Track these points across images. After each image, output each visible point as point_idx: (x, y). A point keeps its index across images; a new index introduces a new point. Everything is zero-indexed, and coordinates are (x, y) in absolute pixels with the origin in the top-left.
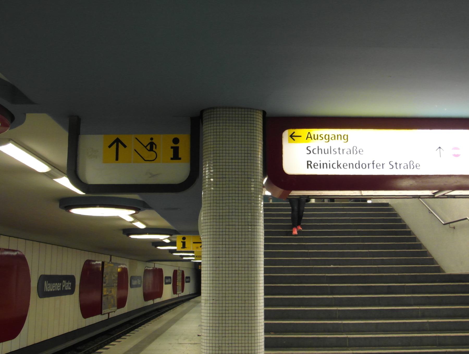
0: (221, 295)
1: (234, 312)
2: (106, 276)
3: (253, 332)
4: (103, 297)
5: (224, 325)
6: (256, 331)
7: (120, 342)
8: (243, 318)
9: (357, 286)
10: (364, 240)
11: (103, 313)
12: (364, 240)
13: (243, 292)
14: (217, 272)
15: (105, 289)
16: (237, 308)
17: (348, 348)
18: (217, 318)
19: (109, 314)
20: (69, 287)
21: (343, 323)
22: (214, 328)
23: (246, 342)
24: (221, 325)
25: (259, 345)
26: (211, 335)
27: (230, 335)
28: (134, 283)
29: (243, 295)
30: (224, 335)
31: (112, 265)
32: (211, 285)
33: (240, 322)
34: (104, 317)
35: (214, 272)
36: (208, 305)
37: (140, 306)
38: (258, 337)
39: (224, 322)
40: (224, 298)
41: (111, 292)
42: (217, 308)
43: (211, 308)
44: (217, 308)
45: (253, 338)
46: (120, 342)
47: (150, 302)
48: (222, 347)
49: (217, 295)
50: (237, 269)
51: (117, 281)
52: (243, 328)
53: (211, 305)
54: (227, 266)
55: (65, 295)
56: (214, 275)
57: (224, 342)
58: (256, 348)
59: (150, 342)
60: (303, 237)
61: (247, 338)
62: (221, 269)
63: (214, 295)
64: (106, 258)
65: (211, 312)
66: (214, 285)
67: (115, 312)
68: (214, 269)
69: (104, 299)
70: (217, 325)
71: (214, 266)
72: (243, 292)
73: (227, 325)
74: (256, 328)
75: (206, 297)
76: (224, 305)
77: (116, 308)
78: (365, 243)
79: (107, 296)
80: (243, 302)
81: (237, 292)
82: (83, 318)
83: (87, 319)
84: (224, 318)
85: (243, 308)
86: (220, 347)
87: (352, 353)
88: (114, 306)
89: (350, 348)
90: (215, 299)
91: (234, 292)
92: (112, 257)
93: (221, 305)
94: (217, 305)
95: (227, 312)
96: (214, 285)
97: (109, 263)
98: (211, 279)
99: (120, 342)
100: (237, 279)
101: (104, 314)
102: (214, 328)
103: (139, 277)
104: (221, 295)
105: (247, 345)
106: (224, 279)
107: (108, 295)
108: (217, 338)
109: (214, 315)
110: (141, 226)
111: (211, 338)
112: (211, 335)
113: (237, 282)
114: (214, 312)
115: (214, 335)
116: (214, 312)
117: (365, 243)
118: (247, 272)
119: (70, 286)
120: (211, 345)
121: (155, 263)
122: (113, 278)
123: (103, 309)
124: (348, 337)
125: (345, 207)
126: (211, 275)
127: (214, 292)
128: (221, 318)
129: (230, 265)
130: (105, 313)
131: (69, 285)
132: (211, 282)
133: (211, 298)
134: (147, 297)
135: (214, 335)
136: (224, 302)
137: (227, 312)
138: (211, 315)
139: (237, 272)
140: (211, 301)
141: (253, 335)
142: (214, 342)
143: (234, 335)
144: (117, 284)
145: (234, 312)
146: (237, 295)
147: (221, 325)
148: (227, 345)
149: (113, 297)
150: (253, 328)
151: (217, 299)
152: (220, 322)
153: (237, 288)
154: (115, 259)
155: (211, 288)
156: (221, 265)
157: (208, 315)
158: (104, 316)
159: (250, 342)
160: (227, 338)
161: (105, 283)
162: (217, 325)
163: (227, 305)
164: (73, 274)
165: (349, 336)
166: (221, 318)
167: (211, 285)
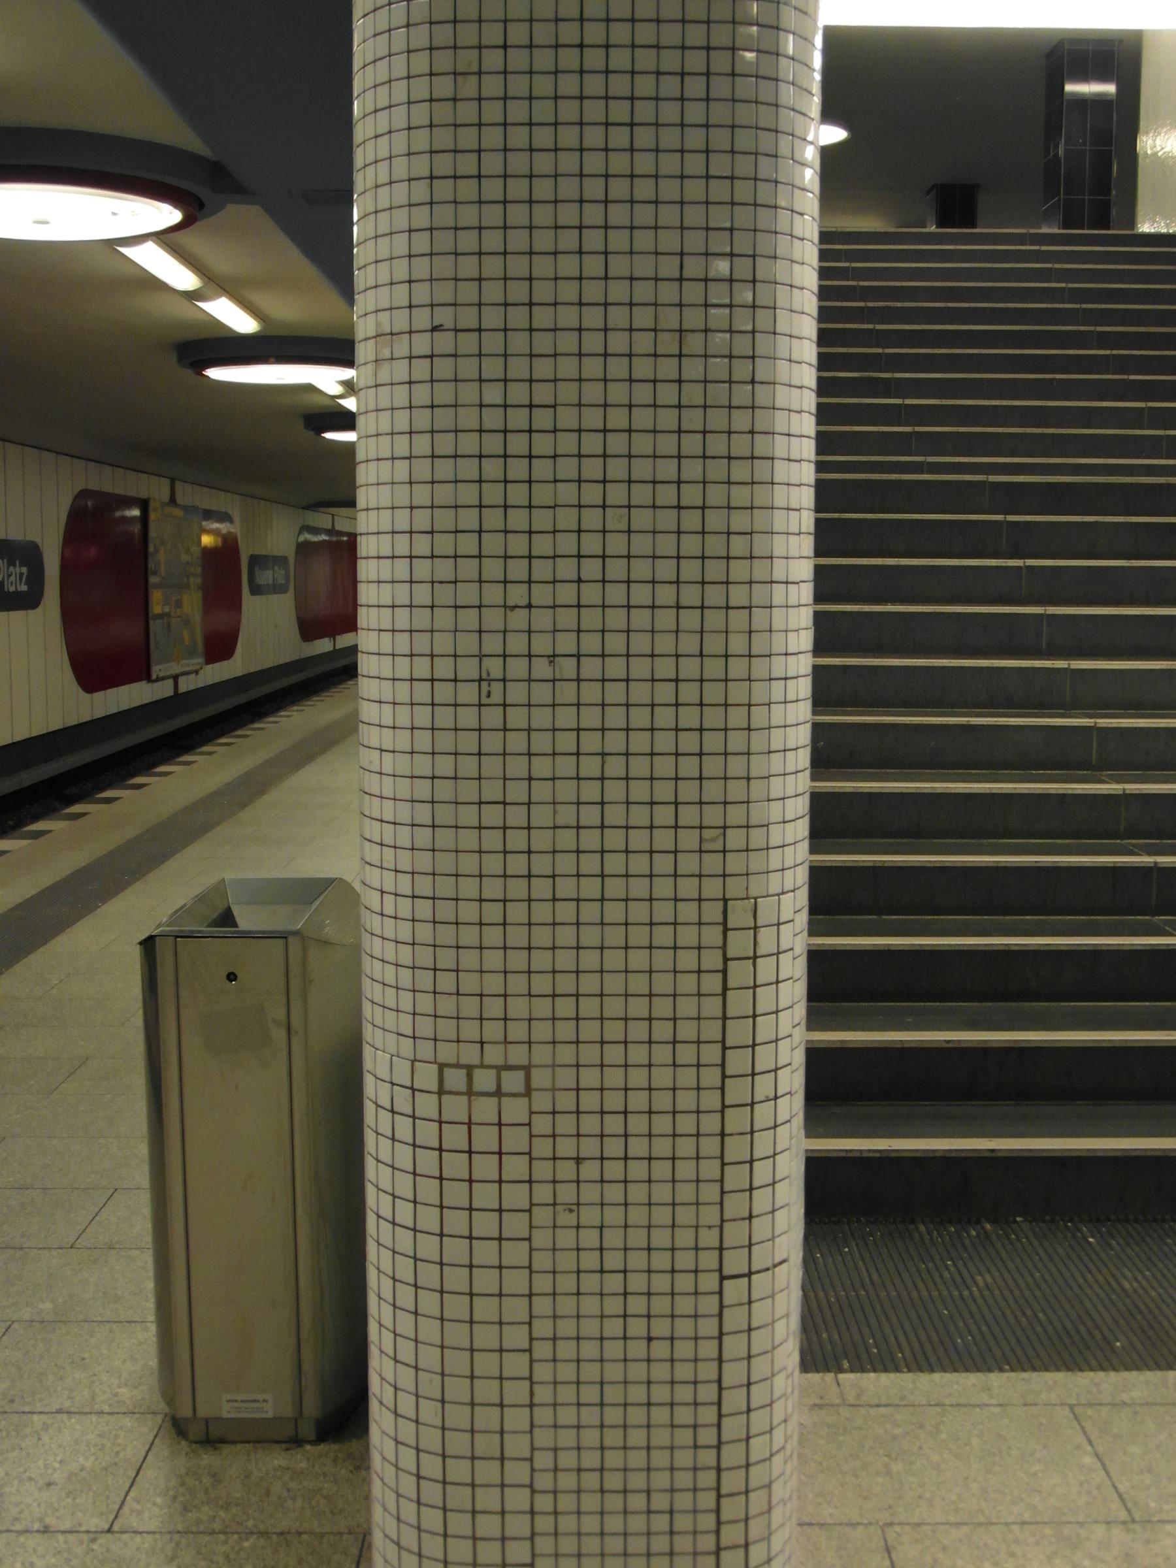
0: (492, 291)
1: (592, 418)
2: (156, 551)
3: (739, 570)
4: (151, 622)
5: (518, 519)
6: (760, 570)
7: (189, 763)
8: (668, 469)
9: (1126, 523)
10: (1123, 365)
11: (154, 677)
12: (1123, 365)
13: (669, 267)
14: (467, 112)
15: (156, 596)
16: (618, 393)
17: (1098, 773)
18: (468, 469)
19: (176, 678)
20: (21, 583)
21: (1072, 667)
22: (445, 544)
23: (689, 644)
24: (493, 519)
25: (778, 672)
26: (423, 594)
27: (567, 594)
28: (265, 577)
29: (668, 292)
30: (517, 594)
31: (178, 513)
32: (422, 217)
33: (642, 494)
34: (164, 690)
35: (444, 112)
36: (400, 370)
37: (287, 657)
38: (778, 615)
39: (518, 494)
40: (518, 317)
41: (179, 604)
42: (469, 393)
43: (422, 394)
44: (469, 393)
45: (738, 619)
46: (189, 763)
47: (323, 646)
48: (504, 680)
49: (468, 292)
50: (619, 85)
51: (199, 570)
52: (667, 545)
53: (422, 369)
54: (543, 59)
55: (8, 611)
56: (444, 138)
57: (517, 644)
58: (759, 692)
59: (298, 766)
60: (880, 351)
61: (690, 619)
62: (493, 85)
63: (445, 292)
64: (156, 489)
65: (423, 419)
66: (445, 216)
67: (197, 672)
68: (444, 87)
69: (155, 627)
70: (469, 519)
71: (444, 61)
72: (669, 267)
73: (542, 520)
74: (760, 545)
75: (384, 317)
76: (519, 368)
77: (201, 660)
78: (1132, 377)
79: (165, 620)
80: (668, 344)
81: (618, 265)
82: (81, 691)
83: (99, 696)
84: (518, 469)
85: (668, 393)
86: (490, 681)
87: (1121, 792)
88: (191, 653)
89: (1104, 773)
90: (449, 324)
91: (594, 266)
92: (178, 484)
93: (493, 368)
94: (468, 368)
95: (543, 419)
96: (445, 216)
97: (163, 504)
98: (421, 166)
99: (189, 763)
100: (619, 163)
101: (158, 680)
102: (445, 544)
103: (281, 561)
104: (492, 291)
105: (689, 668)
106: (519, 163)
107: (168, 615)
108: (469, 619)
109: (445, 444)
110: (243, 323)
111: (422, 619)
112: (423, 594)
113: (619, 188)
114: (444, 418)
115: (445, 594)
116: (444, 418)
117: (1132, 377)
118: (695, 112)
119: (24, 578)
120: (422, 668)
121: (333, 515)
122: (185, 558)
123: (153, 662)
124: (1098, 725)
125: (1044, 248)
126: (421, 140)
127: (445, 265)
128: (492, 469)
129: (569, 59)
130: (161, 675)
131: (21, 575)
132: (421, 191)
133: (422, 318)
134: (309, 629)
135: (445, 594)
136: (519, 342)
137: (543, 419)
138: (422, 444)
139: (620, 112)
140: (422, 344)
141: (738, 595)
142: (443, 643)
143: (591, 594)
144: (199, 580)
145: (592, 418)
146: (619, 292)
147: (493, 519)
148: (542, 669)
149: (187, 622)
150: (738, 545)
151: (468, 318)
152: (493, 494)
153: (619, 240)
154: (187, 494)
155: (422, 243)
156: (493, 59)
157: (402, 445)
158: (156, 685)
159: (714, 644)
160: (542, 619)
161: (155, 573)
162: (469, 519)
163: (543, 368)
164: (33, 536)
165: (1103, 722)
166: (492, 469)
167: (422, 217)
